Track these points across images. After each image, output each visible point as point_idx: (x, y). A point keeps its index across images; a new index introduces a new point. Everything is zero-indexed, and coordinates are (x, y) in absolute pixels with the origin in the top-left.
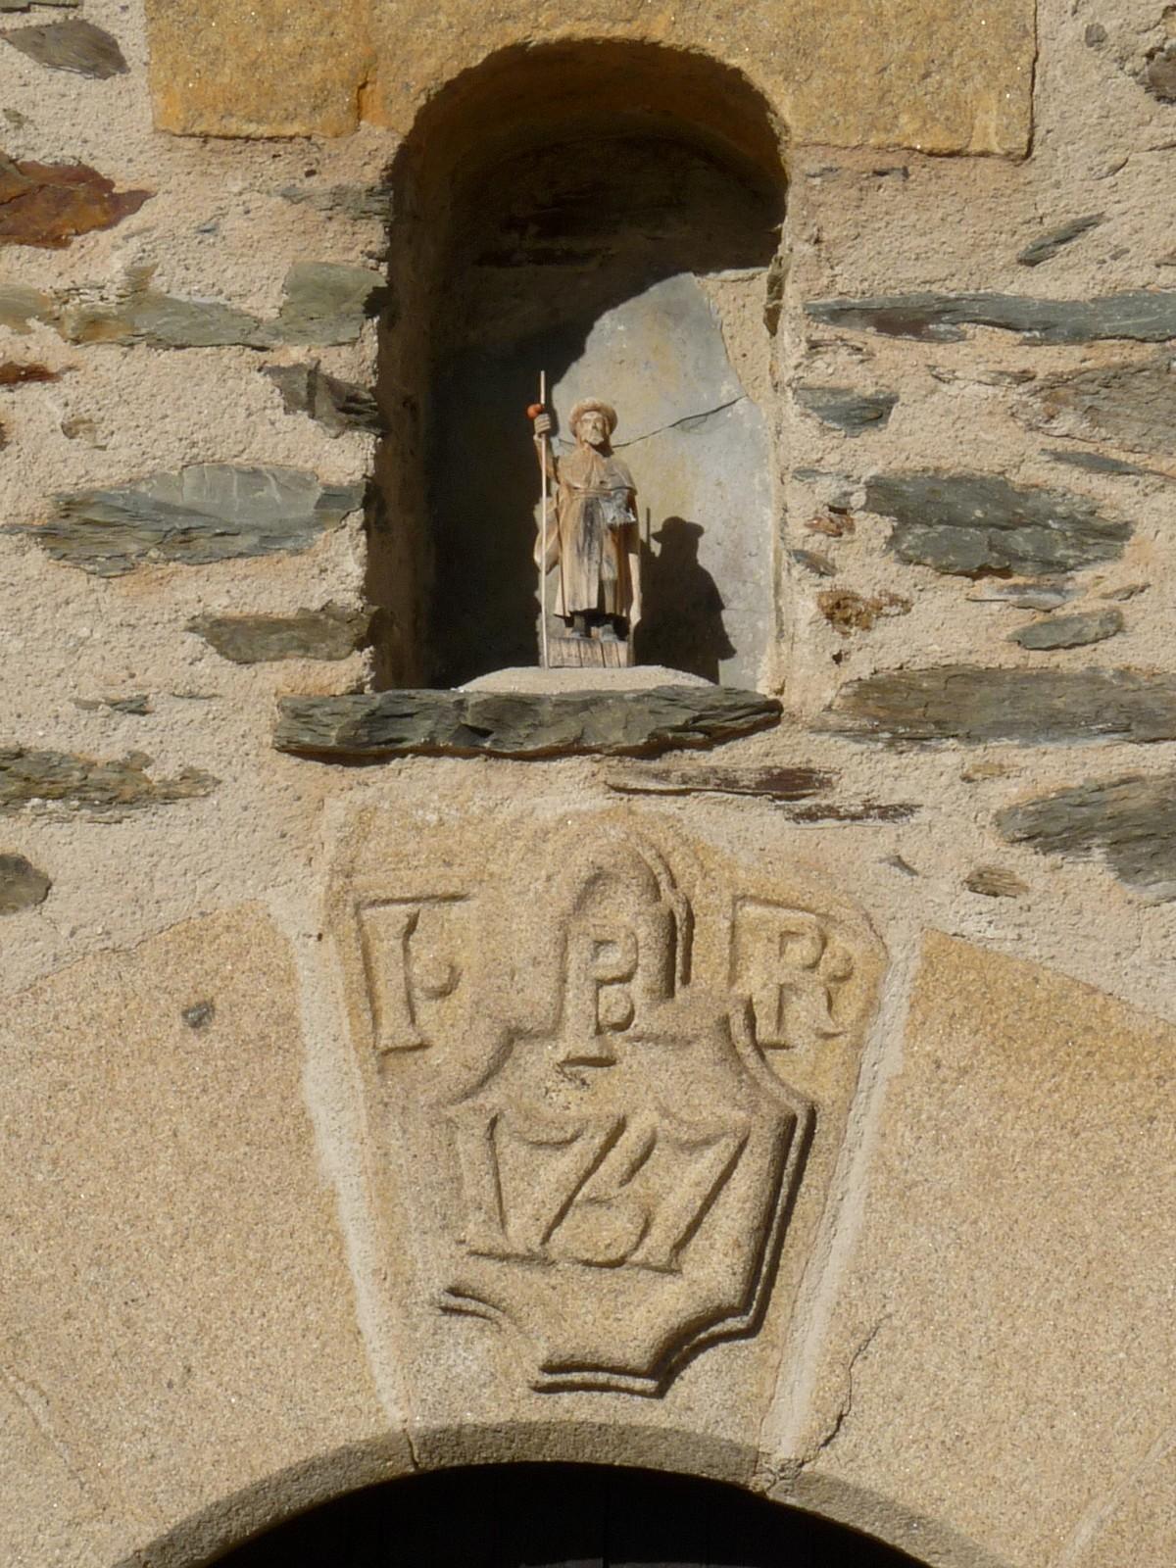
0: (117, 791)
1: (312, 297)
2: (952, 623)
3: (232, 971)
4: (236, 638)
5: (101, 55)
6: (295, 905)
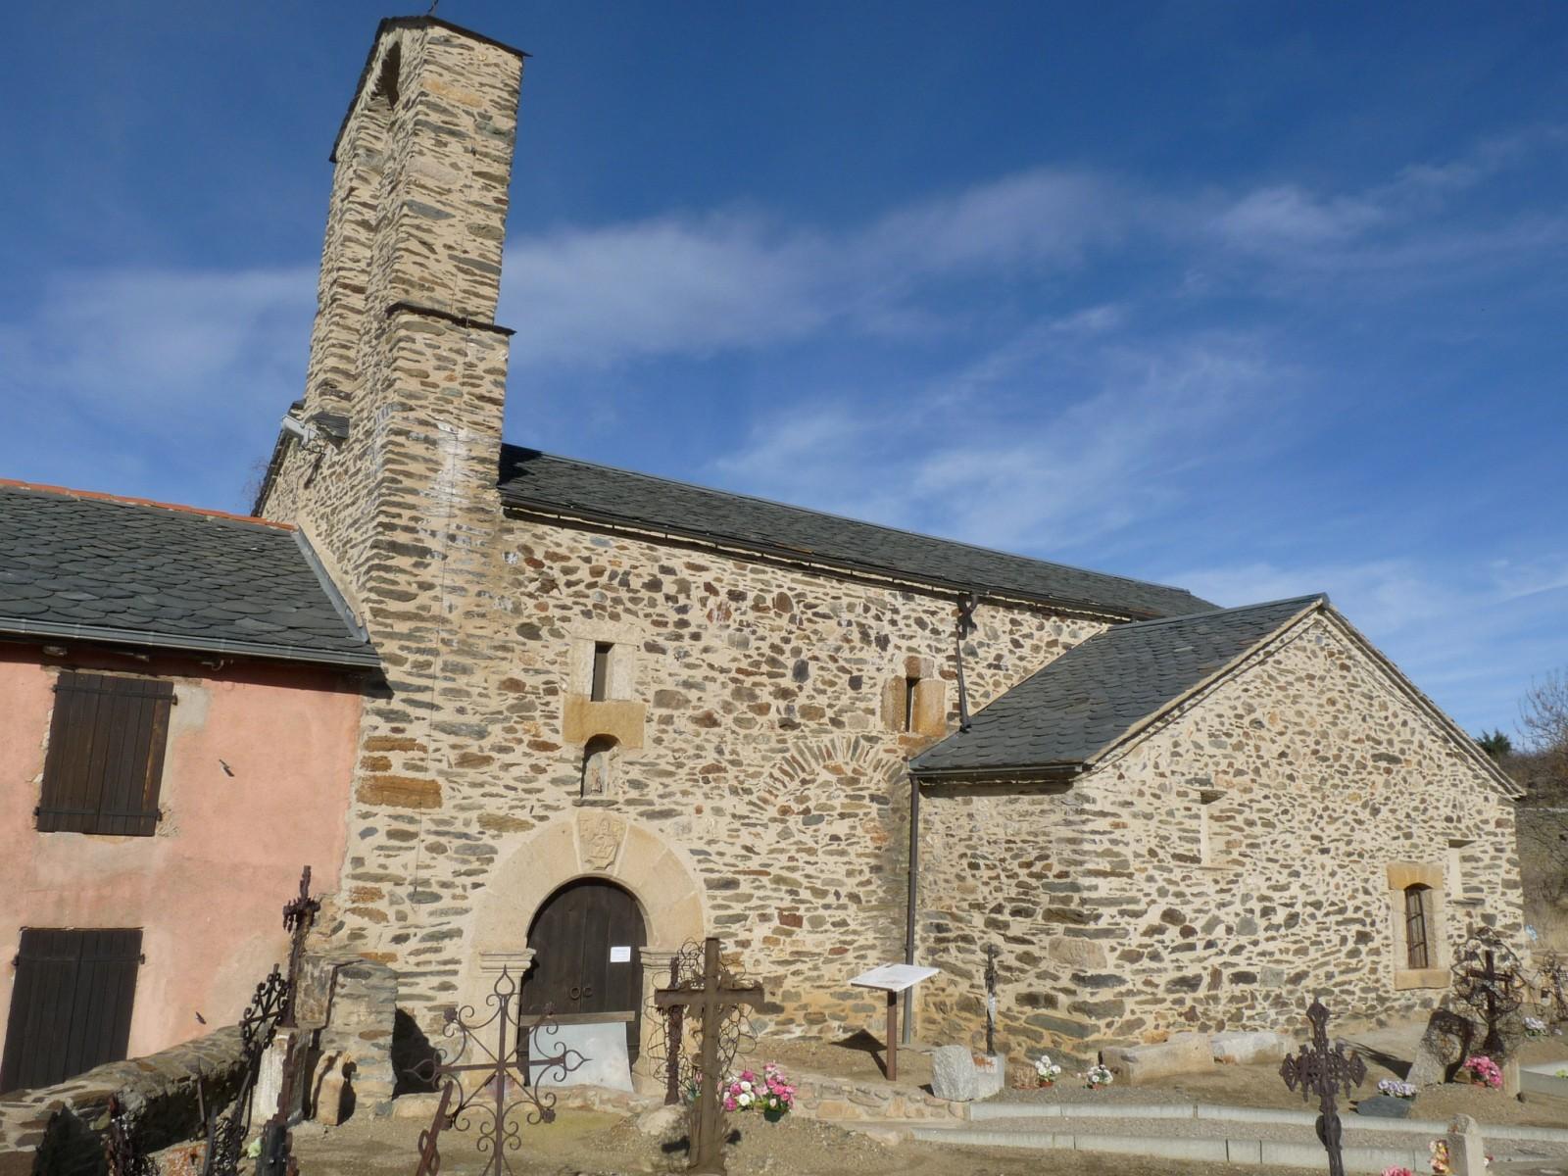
0: (556, 809)
1: (577, 759)
2: (634, 794)
3: (1056, 1059)
4: (569, 793)
5: (557, 732)
6: (573, 821)
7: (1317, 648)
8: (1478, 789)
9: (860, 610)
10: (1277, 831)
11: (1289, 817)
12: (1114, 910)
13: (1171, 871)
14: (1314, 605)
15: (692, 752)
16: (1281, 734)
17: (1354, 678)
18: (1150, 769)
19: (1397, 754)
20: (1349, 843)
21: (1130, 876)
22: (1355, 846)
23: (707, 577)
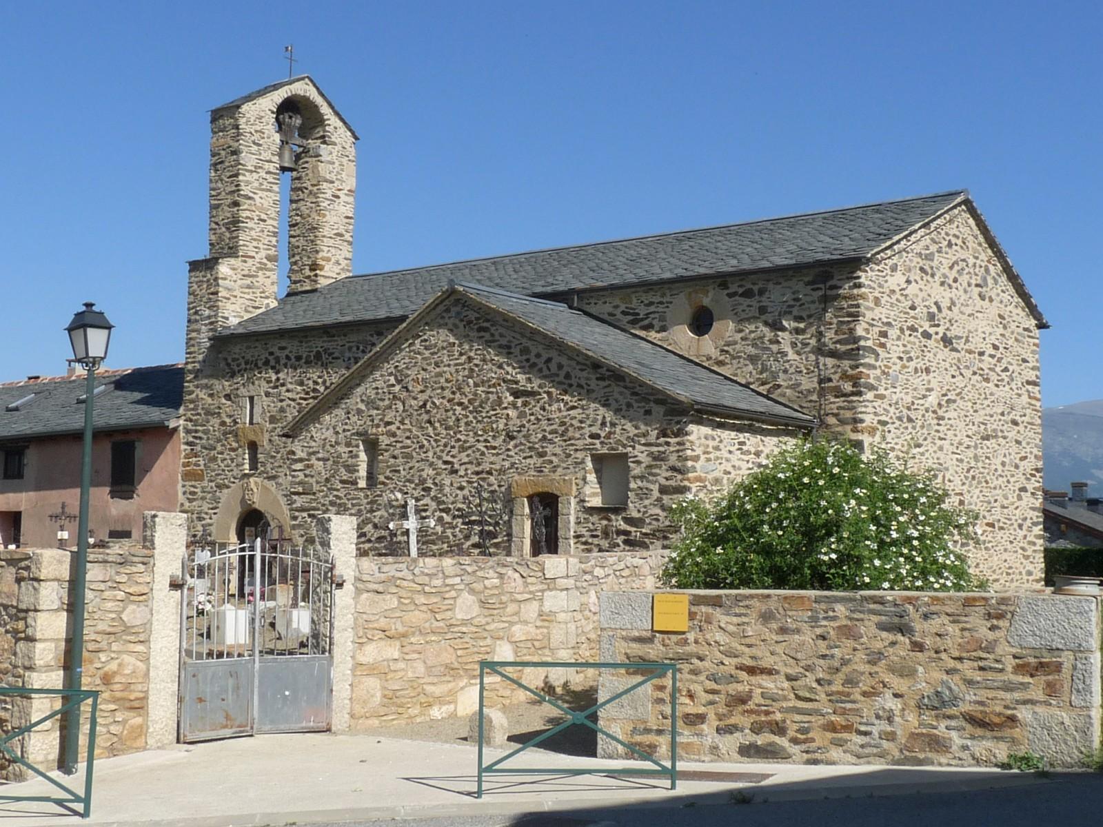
7: (457, 322)
8: (636, 405)
9: (354, 349)
10: (414, 460)
11: (921, 450)
12: (305, 514)
13: (338, 490)
14: (959, 200)
15: (282, 445)
16: (422, 392)
17: (492, 335)
18: (331, 430)
19: (536, 388)
20: (479, 464)
21: (314, 494)
22: (486, 467)
23: (287, 352)
